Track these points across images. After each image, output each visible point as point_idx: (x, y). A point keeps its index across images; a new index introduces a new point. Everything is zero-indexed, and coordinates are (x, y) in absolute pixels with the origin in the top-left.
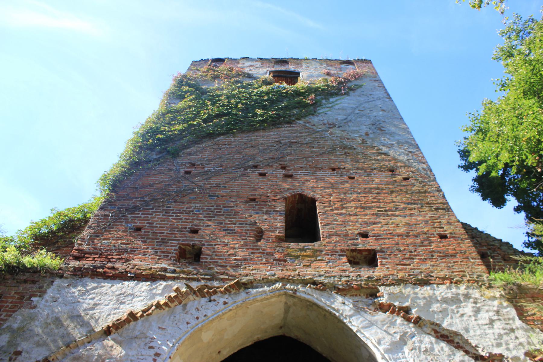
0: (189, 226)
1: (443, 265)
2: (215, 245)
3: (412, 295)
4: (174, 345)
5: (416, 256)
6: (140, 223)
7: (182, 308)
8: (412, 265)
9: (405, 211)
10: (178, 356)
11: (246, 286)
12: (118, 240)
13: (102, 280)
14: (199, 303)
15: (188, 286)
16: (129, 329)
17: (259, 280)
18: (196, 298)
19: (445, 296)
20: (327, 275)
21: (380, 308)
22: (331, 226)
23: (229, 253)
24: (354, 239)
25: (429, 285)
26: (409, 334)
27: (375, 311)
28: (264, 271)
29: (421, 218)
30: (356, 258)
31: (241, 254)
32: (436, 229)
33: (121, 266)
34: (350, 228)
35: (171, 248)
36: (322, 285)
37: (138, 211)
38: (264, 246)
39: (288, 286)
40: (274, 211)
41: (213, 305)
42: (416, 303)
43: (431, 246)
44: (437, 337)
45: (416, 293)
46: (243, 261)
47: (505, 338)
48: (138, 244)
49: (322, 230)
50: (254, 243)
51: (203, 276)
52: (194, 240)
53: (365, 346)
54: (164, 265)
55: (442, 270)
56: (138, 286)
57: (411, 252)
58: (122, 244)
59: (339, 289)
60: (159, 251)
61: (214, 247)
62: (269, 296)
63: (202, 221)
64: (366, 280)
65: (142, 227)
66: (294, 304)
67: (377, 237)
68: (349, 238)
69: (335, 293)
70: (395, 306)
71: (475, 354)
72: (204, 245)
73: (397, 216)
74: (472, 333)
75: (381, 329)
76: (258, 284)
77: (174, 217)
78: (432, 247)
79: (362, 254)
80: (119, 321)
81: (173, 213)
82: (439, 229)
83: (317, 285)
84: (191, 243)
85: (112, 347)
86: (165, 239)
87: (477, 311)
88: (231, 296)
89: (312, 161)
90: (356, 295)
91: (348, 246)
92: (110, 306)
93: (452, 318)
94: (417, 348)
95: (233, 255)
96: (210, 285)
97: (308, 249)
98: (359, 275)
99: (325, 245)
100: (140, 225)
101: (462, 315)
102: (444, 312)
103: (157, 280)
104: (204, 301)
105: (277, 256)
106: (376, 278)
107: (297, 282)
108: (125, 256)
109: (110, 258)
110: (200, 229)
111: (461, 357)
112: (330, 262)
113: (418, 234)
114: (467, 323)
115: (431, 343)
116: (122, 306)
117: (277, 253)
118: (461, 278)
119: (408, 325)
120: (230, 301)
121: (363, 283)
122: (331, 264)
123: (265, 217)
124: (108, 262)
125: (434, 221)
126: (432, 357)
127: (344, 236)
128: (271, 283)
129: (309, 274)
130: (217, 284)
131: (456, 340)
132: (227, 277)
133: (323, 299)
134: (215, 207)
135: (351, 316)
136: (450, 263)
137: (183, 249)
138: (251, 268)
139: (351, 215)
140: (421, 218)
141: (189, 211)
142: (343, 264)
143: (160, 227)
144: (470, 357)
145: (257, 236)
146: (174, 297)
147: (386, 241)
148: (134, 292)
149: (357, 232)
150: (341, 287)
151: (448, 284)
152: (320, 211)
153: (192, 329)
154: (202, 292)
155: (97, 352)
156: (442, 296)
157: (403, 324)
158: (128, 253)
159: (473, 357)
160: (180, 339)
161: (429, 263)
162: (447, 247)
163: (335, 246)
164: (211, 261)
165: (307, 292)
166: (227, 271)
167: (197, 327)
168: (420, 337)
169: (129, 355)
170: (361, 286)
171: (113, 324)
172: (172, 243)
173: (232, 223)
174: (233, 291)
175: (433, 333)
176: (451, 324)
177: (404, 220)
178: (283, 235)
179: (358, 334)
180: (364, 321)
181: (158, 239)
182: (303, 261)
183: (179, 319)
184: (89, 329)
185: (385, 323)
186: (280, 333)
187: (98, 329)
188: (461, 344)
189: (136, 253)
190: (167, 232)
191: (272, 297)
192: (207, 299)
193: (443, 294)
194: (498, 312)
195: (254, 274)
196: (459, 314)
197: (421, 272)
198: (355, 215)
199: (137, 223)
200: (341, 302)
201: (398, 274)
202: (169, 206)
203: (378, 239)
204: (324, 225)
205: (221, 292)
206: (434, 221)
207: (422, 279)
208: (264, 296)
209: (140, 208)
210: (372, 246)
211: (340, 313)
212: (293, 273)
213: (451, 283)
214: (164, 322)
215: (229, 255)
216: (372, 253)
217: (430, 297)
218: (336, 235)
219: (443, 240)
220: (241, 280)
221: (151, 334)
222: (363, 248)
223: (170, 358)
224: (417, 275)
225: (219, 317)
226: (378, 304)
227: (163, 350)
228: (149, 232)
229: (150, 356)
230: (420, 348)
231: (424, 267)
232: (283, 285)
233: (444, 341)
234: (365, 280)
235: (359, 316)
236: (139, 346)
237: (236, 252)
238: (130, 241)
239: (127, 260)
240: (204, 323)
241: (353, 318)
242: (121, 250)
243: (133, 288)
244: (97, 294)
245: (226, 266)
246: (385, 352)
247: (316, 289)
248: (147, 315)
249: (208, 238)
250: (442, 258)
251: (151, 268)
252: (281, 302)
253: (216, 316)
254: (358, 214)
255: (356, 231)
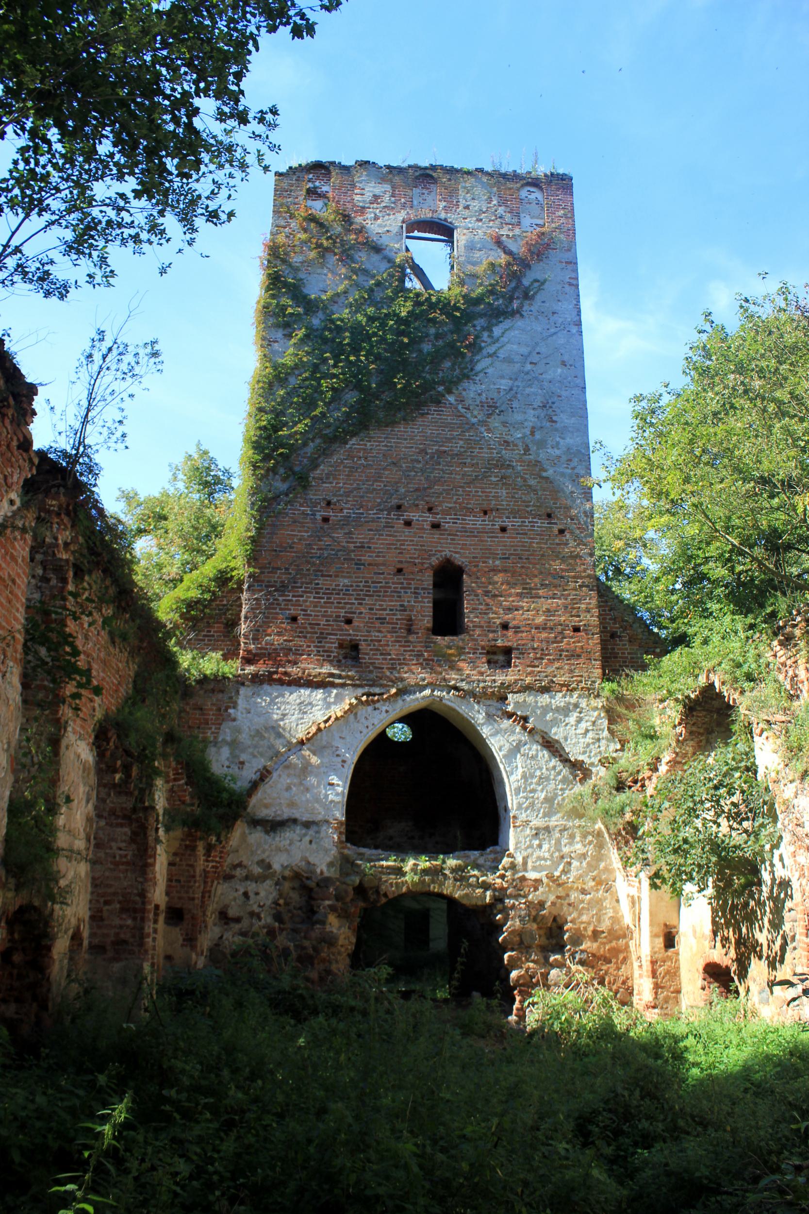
47: (592, 746)
54: (327, 669)
87: (579, 720)
89: (349, 425)
102: (555, 722)
113: (555, 625)
176: (555, 734)
194: (594, 723)
221: (335, 744)
243: (309, 696)
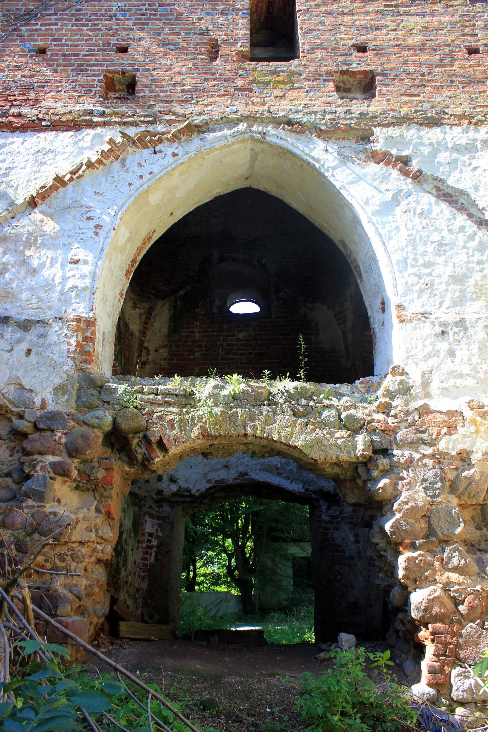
0: (114, 40)
1: (464, 96)
2: (154, 70)
3: (416, 141)
4: (116, 214)
5: (429, 81)
6: (41, 40)
7: (120, 164)
8: (422, 95)
9: (426, 6)
10: (123, 226)
11: (200, 129)
12: (17, 70)
13: (9, 134)
14: (141, 157)
15: (124, 135)
16: (58, 198)
17: (217, 120)
18: (137, 150)
19: (458, 143)
20: (306, 110)
21: (373, 157)
22: (314, 33)
23: (175, 80)
24: (346, 55)
25: (440, 126)
26: (404, 191)
27: (365, 161)
28: (223, 107)
29: (447, 18)
30: (347, 83)
31: (190, 83)
32: (466, 37)
34: (343, 36)
35: (93, 78)
36: (300, 125)
37: (35, 20)
38: (221, 67)
39: (255, 128)
40: (233, 10)
41: (160, 159)
42: (420, 150)
43: (452, 66)
44: (438, 197)
45: (420, 138)
46: (194, 93)
48: (46, 76)
49: (303, 41)
50: (207, 63)
51: (142, 119)
52: (123, 64)
53: (349, 206)
55: (460, 104)
56: (58, 138)
57: (423, 75)
58: (23, 76)
59: (321, 130)
60: (77, 84)
61: (152, 72)
62: (230, 143)
63: (131, 32)
64: (357, 118)
65: (46, 47)
66: (263, 151)
67: (379, 51)
68: (339, 53)
69: (315, 136)
70: (391, 155)
71: (479, 218)
72: (138, 70)
73: (412, 15)
74: (481, 192)
75: (370, 185)
76: (215, 126)
77: (89, 27)
78: (454, 68)
79: (355, 78)
80: (44, 190)
81: (86, 20)
82: (469, 38)
83: (293, 125)
84: (120, 68)
85: (42, 221)
86: (83, 65)
88: (182, 144)
90: (343, 139)
91: (337, 65)
92: (28, 170)
93: (461, 172)
94: (412, 210)
95: (180, 84)
96: (152, 130)
97: (281, 71)
98: (349, 110)
99: (305, 65)
100: (42, 43)
101: (475, 168)
102: (452, 164)
103: (82, 128)
104: (147, 153)
105: (239, 83)
106: (371, 115)
107: (266, 121)
108: (32, 95)
109: (12, 101)
110: (130, 45)
111: (463, 222)
112: (310, 90)
113: (438, 46)
114: (478, 180)
115: (430, 204)
116: (43, 168)
117: (239, 78)
118: (484, 116)
119: (404, 180)
120: (180, 151)
121: (353, 122)
122: (312, 93)
123: (221, 20)
124: (11, 107)
125: (466, 23)
126: (428, 221)
127: (333, 49)
128: (232, 124)
129: (283, 110)
130: (162, 128)
131: (461, 201)
132: (173, 118)
133: (299, 145)
134: (147, 6)
135: (334, 168)
136: (475, 93)
137: (111, 78)
138: (205, 102)
139: (345, 14)
140: (447, 18)
141: (110, 15)
142: (328, 94)
143: (72, 46)
144: (472, 222)
145: (211, 52)
146: (108, 151)
147: (391, 58)
148: (54, 147)
149: (351, 42)
150: (323, 128)
151: (465, 125)
152: (301, 8)
153: (136, 191)
154: (143, 141)
155: (26, 229)
156: (454, 142)
157: (399, 180)
158: (36, 91)
159: (476, 222)
160: (123, 205)
161: (447, 93)
162: (475, 69)
163: (319, 66)
164: (150, 94)
165: (280, 135)
166: (173, 109)
167: (142, 188)
168: (418, 196)
169: (64, 230)
170: (351, 126)
171: (38, 193)
172: (94, 70)
173: (174, 33)
174: (183, 138)
175: (434, 191)
177: (422, 22)
178: (247, 49)
179: (342, 192)
180: (350, 174)
181: (73, 65)
182: (275, 91)
183: (119, 180)
184: (9, 201)
185: (377, 177)
186: (245, 184)
187: (20, 201)
188: (466, 205)
189: (46, 89)
190: (83, 53)
191: (234, 143)
192: (150, 151)
193: (456, 139)
195: (209, 112)
196: (471, 167)
197: (432, 107)
198: (350, 14)
199: (37, 40)
200: (323, 148)
201: (401, 110)
202: (78, 7)
203: (380, 54)
204: (304, 33)
205: (168, 140)
206: (466, 23)
207: (432, 118)
208: (223, 143)
209: (37, 14)
210: (370, 65)
211: (321, 163)
212: (261, 109)
213: (470, 123)
214: (100, 185)
215: (174, 84)
216: (370, 76)
217: (439, 143)
218: (321, 49)
219: (472, 56)
220: (193, 121)
221: (86, 201)
222: (358, 69)
223: (114, 229)
224: (426, 111)
225: (169, 174)
226: (369, 151)
227: (104, 220)
228: (57, 55)
229: (90, 229)
230: (415, 210)
231: (438, 99)
232: (248, 126)
233: (446, 201)
234: (356, 117)
235: (345, 168)
236: (74, 217)
237: (183, 79)
238: (34, 71)
239: (37, 101)
240: (150, 182)
241: (338, 170)
242: (24, 86)
244: (7, 154)
245: (172, 101)
246: (372, 215)
247: (291, 131)
248: (77, 177)
249: (143, 59)
250: (465, 85)
251: (71, 112)
252: (246, 148)
253: (164, 172)
254: (356, 11)
255: (350, 41)
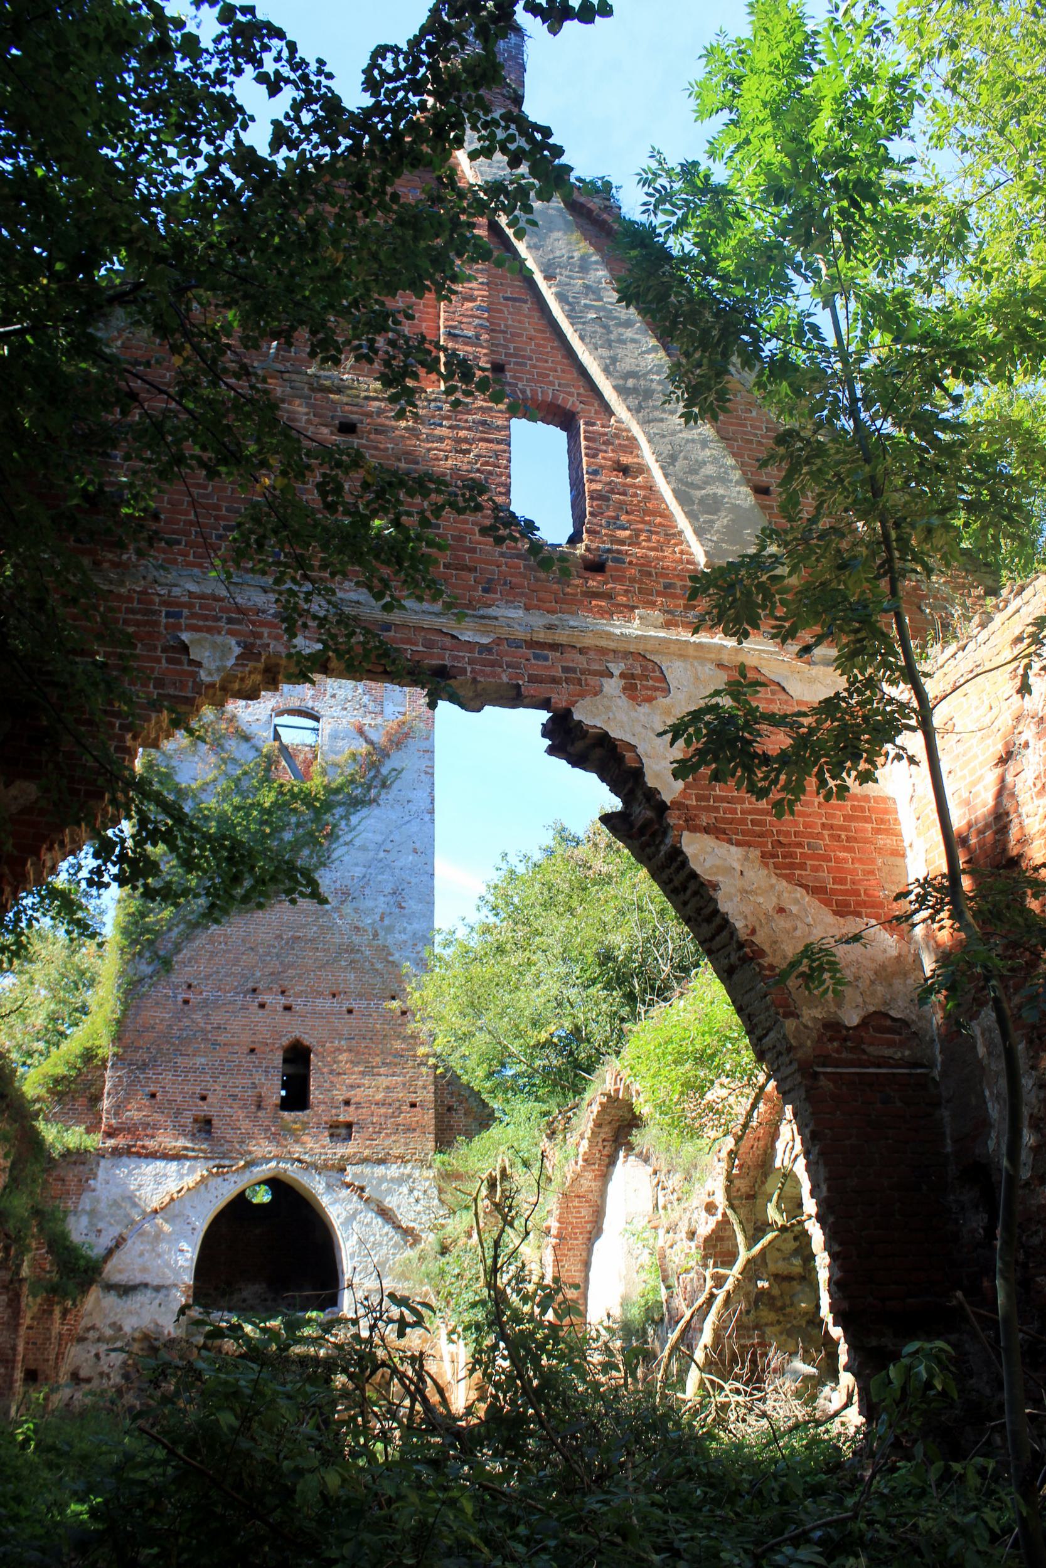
33: (151, 1144)
102: (389, 1191)
